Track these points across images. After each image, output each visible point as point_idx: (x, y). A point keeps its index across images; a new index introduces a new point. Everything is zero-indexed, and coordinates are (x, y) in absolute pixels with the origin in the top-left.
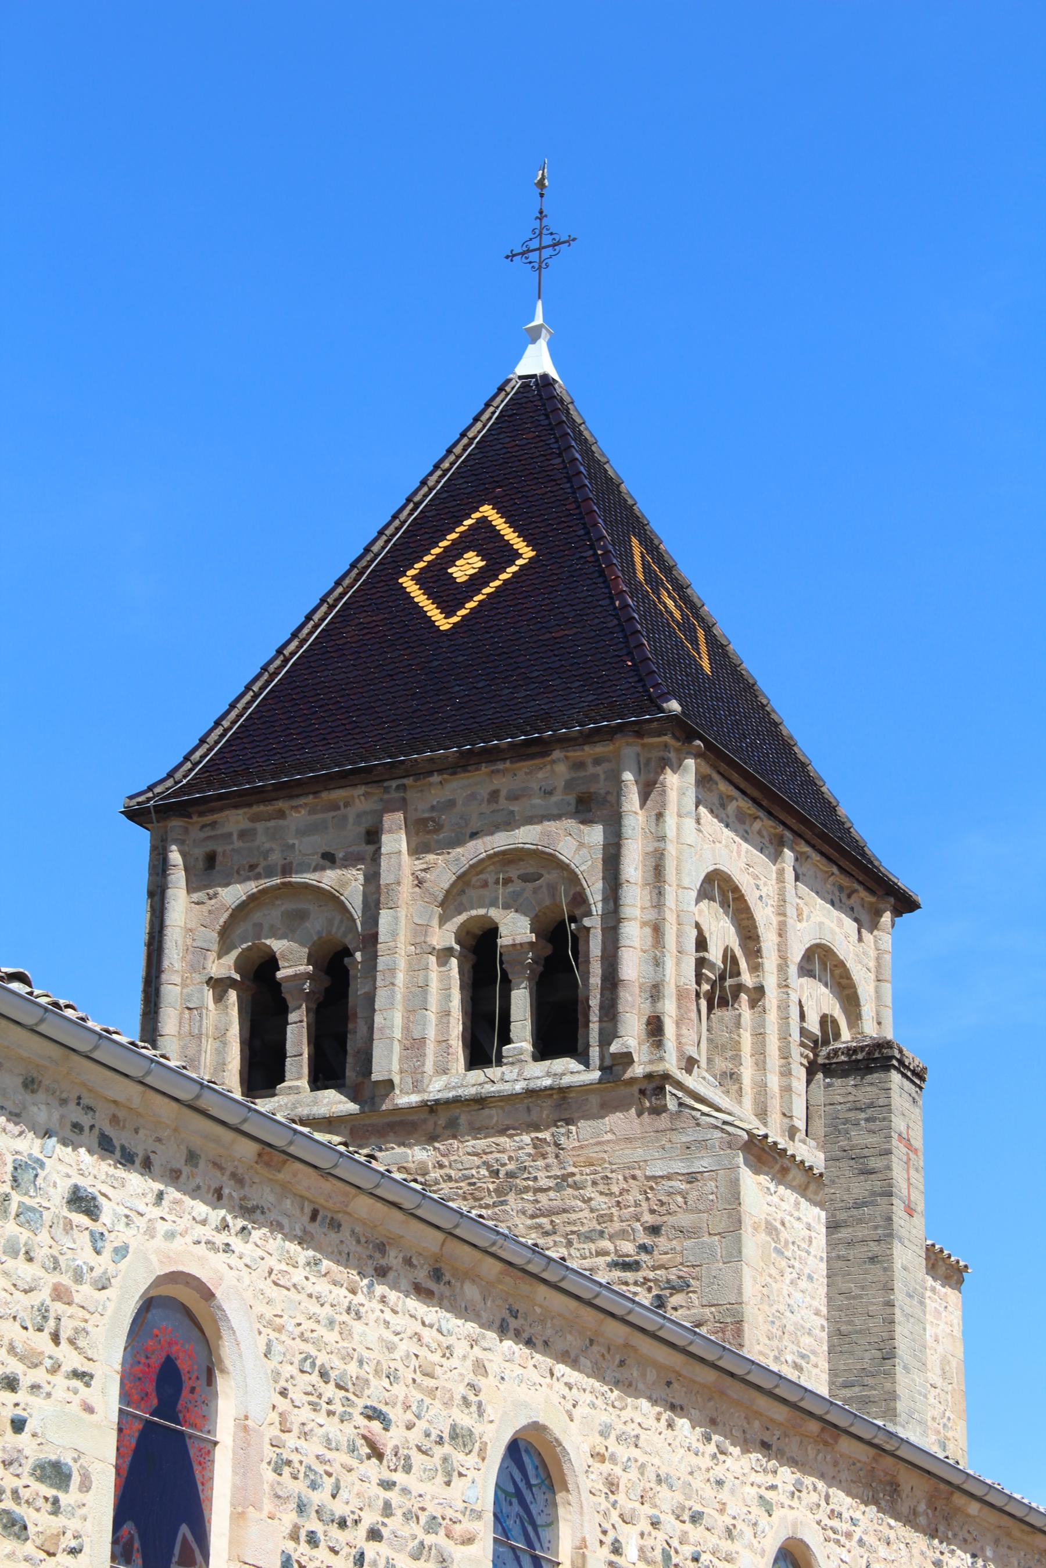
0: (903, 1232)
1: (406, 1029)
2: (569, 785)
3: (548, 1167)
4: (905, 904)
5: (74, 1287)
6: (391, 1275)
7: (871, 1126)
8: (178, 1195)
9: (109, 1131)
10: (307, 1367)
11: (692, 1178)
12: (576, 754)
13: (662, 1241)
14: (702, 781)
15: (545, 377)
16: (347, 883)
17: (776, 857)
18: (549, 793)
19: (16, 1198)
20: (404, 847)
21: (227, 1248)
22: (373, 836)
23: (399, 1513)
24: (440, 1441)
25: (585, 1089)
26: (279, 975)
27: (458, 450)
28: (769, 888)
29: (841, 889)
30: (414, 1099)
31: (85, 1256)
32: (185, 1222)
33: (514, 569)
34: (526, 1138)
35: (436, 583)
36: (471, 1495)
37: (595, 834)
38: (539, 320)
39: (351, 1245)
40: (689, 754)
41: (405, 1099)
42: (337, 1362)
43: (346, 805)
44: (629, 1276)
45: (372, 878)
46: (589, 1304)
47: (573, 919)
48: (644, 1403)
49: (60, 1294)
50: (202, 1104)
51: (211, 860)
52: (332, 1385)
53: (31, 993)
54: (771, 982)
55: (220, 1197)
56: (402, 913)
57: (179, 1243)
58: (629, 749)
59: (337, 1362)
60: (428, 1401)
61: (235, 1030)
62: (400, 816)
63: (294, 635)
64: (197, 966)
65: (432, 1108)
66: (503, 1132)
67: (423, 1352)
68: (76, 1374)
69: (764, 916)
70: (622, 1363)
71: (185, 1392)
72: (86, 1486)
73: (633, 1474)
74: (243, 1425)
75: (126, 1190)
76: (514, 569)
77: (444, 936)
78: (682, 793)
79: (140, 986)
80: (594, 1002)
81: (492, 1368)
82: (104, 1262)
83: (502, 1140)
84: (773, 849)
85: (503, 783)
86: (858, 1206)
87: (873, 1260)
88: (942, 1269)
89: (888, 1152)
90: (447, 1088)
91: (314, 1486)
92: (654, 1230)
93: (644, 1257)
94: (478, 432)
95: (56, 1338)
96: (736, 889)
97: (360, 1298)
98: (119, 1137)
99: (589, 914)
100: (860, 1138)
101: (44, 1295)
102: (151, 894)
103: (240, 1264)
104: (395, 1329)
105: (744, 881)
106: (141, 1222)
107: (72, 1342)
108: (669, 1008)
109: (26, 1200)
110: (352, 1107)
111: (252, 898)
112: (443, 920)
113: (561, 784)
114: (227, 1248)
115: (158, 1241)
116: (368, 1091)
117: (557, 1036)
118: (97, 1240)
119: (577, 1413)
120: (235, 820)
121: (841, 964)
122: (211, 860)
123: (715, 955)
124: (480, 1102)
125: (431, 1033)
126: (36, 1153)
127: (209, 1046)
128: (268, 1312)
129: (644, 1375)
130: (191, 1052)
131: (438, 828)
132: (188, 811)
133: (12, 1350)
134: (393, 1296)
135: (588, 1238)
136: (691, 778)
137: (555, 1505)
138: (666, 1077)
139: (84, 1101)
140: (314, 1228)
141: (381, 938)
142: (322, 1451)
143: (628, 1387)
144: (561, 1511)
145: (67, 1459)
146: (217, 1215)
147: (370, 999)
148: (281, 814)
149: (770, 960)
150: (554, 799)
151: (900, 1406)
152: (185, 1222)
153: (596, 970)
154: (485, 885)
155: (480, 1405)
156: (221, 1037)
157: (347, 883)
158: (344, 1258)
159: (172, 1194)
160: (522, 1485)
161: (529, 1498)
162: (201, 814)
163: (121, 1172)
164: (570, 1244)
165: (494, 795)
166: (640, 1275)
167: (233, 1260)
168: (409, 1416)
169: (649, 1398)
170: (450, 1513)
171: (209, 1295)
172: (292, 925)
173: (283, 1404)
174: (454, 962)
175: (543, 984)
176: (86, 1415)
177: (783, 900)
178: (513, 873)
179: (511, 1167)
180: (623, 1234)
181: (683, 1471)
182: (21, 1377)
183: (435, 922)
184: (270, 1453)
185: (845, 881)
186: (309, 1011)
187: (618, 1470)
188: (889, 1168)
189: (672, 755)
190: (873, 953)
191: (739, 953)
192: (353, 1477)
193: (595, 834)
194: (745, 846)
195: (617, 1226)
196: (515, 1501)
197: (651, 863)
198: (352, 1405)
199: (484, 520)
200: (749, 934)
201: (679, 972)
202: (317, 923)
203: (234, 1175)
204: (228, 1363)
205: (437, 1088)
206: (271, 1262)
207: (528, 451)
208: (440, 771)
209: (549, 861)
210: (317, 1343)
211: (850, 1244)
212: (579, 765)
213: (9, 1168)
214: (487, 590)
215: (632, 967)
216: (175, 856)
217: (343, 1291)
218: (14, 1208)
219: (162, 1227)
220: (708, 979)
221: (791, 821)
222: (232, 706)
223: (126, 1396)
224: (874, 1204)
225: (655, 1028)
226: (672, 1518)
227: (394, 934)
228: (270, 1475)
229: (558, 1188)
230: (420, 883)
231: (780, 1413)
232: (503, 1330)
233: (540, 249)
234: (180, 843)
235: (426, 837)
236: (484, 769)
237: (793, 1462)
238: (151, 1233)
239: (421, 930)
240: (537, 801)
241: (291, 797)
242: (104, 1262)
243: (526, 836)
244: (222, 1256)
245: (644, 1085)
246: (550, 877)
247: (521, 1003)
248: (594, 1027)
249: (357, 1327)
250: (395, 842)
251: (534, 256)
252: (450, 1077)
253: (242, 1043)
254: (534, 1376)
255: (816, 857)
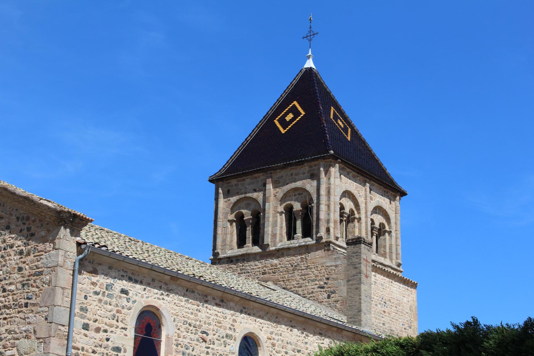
0: (364, 282)
1: (272, 231)
2: (309, 171)
3: (304, 264)
4: (403, 194)
5: (122, 310)
6: (209, 302)
7: (357, 257)
8: (150, 288)
9: (131, 276)
10: (185, 323)
11: (336, 266)
12: (310, 164)
13: (329, 282)
14: (340, 169)
15: (311, 68)
16: (258, 196)
17: (364, 185)
18: (304, 173)
19: (107, 292)
20: (271, 187)
21: (163, 299)
22: (265, 185)
23: (211, 354)
24: (223, 337)
25: (312, 245)
26: (244, 219)
27: (290, 87)
28: (362, 193)
29: (385, 191)
30: (274, 248)
31: (125, 303)
32: (152, 294)
33: (300, 117)
34: (299, 257)
35: (283, 122)
36: (232, 349)
37: (315, 183)
38: (310, 54)
39: (198, 296)
40: (337, 163)
41: (272, 248)
42: (193, 322)
43: (259, 177)
44: (322, 290)
45: (264, 195)
46: (265, 305)
47: (310, 204)
48: (283, 326)
49: (118, 311)
50: (153, 269)
51: (229, 191)
52: (192, 327)
53: (107, 250)
54: (363, 216)
55: (161, 288)
56: (271, 203)
57: (150, 299)
58: (322, 163)
59: (193, 322)
60: (219, 329)
61: (235, 232)
62: (270, 180)
63: (250, 135)
64: (226, 217)
65: (278, 250)
66: (294, 256)
67: (218, 318)
68: (122, 328)
69: (361, 201)
70: (277, 317)
71: (153, 331)
72: (125, 351)
73: (280, 342)
74: (167, 337)
75: (135, 289)
76: (300, 117)
77: (281, 209)
78: (335, 173)
79: (213, 222)
80: (314, 224)
81: (238, 321)
82: (130, 304)
83: (294, 258)
84: (364, 184)
85: (294, 171)
86: (354, 276)
87: (357, 289)
88: (410, 284)
89: (360, 263)
90: (281, 245)
91: (187, 349)
92: (328, 279)
93: (325, 285)
94: (295, 82)
95: (117, 321)
96: (353, 194)
97: (200, 307)
98: (133, 277)
99: (313, 203)
100: (355, 260)
101: (114, 312)
102: (215, 200)
103: (167, 302)
104: (210, 314)
105: (355, 192)
106: (140, 295)
107: (121, 321)
108: (332, 225)
109: (110, 292)
110: (260, 250)
111: (238, 200)
112: (281, 205)
113: (307, 171)
114: (163, 299)
115: (144, 299)
116: (264, 247)
117: (307, 233)
118: (128, 300)
119: (263, 329)
120: (234, 182)
121: (385, 210)
122: (229, 191)
123: (347, 210)
124: (289, 249)
125: (278, 232)
126: (112, 282)
127: (229, 236)
128: (174, 312)
129: (283, 320)
130: (224, 238)
131: (279, 183)
132: (223, 180)
133: (106, 324)
134: (209, 306)
135: (313, 281)
136: (337, 168)
137: (258, 350)
138: (330, 242)
139: (125, 270)
140: (187, 293)
141: (266, 210)
142: (189, 341)
143: (279, 323)
144: (259, 351)
145: (120, 346)
146: (160, 292)
147: (264, 224)
148: (244, 180)
149: (363, 211)
150: (305, 175)
151: (362, 323)
152: (152, 294)
153: (315, 216)
154: (290, 196)
155: (234, 329)
156: (232, 234)
157: (258, 196)
158: (196, 299)
159: (148, 288)
160: (248, 346)
161: (250, 348)
162: (226, 180)
163: (134, 285)
164: (309, 282)
165: (292, 174)
166: (325, 289)
167: (165, 301)
168: (214, 332)
169: (285, 325)
170: (225, 353)
171: (158, 309)
172: (247, 207)
173: (178, 332)
174: (284, 215)
175: (303, 219)
176: (125, 337)
177: (366, 196)
178: (297, 193)
179: (296, 264)
180: (321, 280)
181: (295, 341)
182: (257, 332)
183: (279, 205)
184: (175, 342)
185: (386, 190)
186: (250, 227)
187: (275, 342)
188: (360, 267)
189: (333, 164)
190: (394, 207)
191: (354, 209)
192: (198, 346)
193: (315, 183)
194: (355, 183)
195: (319, 278)
196: (246, 350)
197: (327, 190)
198: (198, 331)
199: (294, 105)
200: (357, 205)
201: (335, 216)
202: (253, 206)
203: (165, 283)
204: (164, 323)
205: (279, 246)
206: (176, 301)
207: (308, 89)
208: (279, 169)
209: (305, 190)
210: (188, 318)
211: (352, 285)
212: (311, 167)
213: (105, 286)
214: (293, 123)
215: (323, 216)
216: (220, 191)
217: (196, 306)
218: (106, 294)
219: (145, 296)
220: (345, 217)
221: (368, 176)
222: (235, 153)
223: (136, 331)
224: (357, 275)
225: (328, 230)
226: (292, 352)
227: (269, 209)
228: (175, 347)
229: (306, 269)
230: (275, 196)
231: (325, 326)
232: (241, 312)
233: (310, 36)
234: (222, 188)
235: (277, 184)
236: (289, 168)
237: (329, 337)
238: (142, 297)
239: (276, 207)
240: (301, 176)
241: (246, 176)
242: (130, 304)
243: (299, 184)
244: (162, 301)
245: (326, 244)
246: (305, 194)
247: (299, 224)
248: (314, 230)
249: (199, 314)
250: (270, 186)
251: (309, 38)
252: (283, 242)
253: (237, 235)
254: (251, 322)
255: (376, 184)
